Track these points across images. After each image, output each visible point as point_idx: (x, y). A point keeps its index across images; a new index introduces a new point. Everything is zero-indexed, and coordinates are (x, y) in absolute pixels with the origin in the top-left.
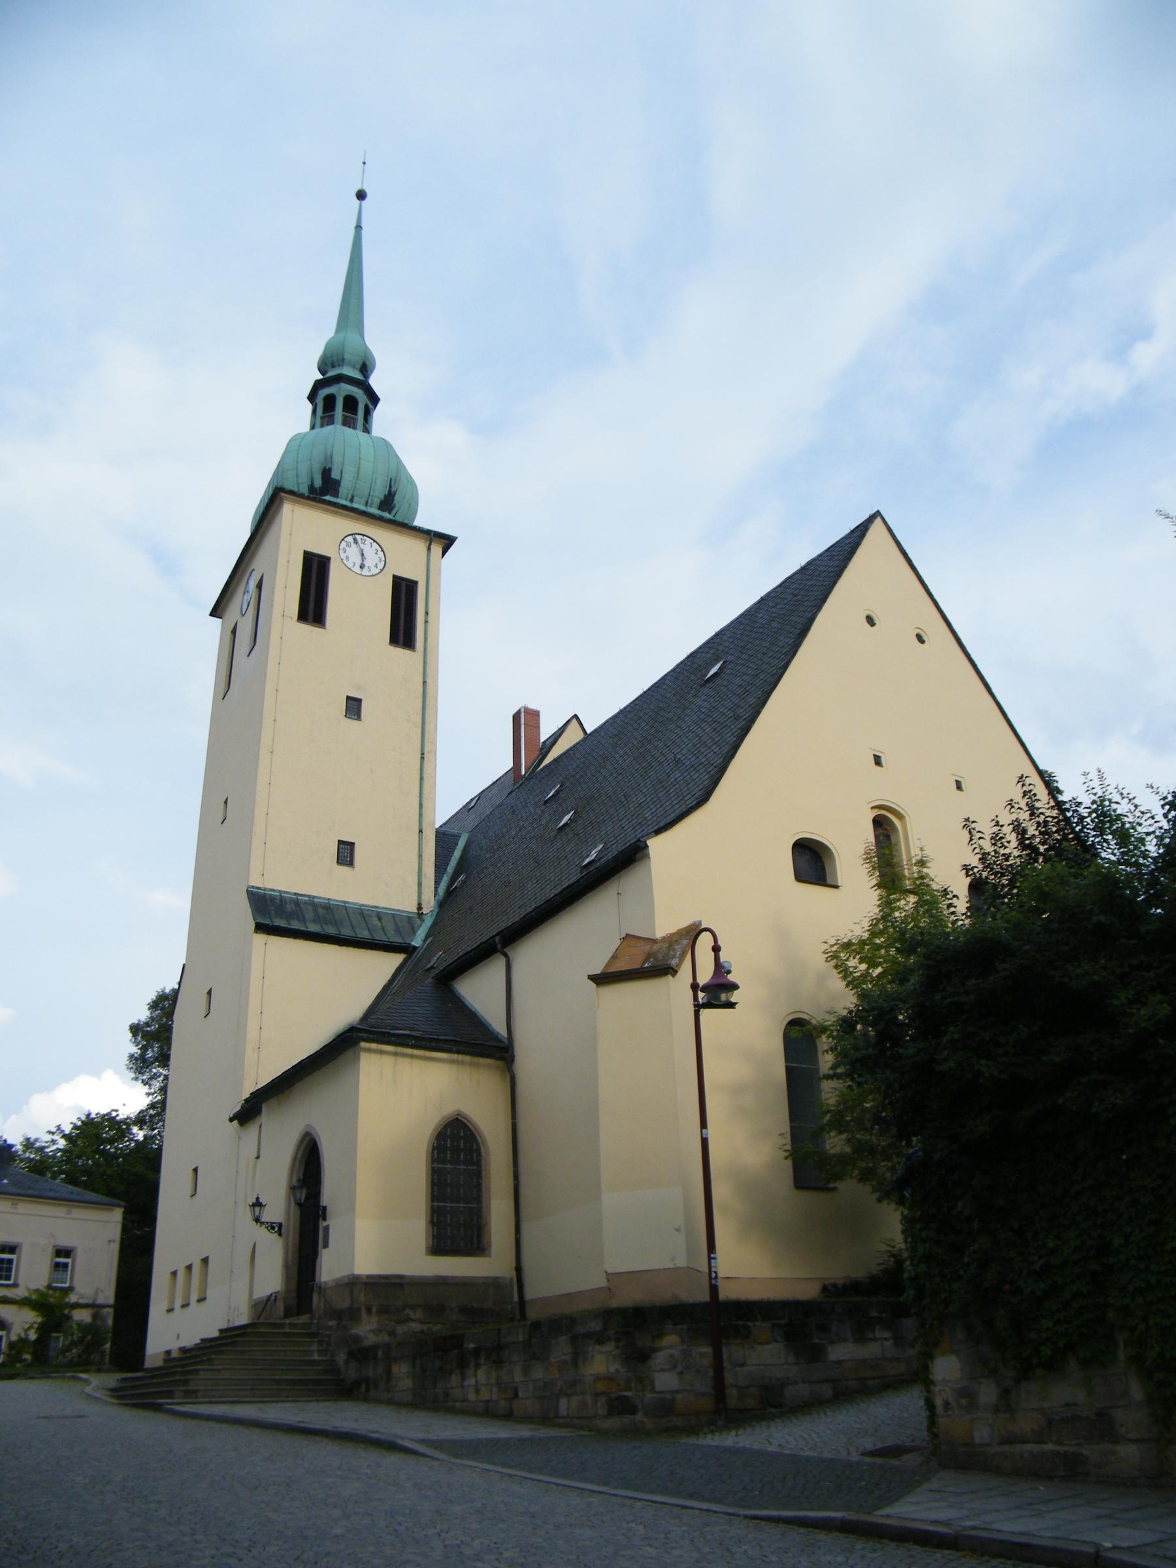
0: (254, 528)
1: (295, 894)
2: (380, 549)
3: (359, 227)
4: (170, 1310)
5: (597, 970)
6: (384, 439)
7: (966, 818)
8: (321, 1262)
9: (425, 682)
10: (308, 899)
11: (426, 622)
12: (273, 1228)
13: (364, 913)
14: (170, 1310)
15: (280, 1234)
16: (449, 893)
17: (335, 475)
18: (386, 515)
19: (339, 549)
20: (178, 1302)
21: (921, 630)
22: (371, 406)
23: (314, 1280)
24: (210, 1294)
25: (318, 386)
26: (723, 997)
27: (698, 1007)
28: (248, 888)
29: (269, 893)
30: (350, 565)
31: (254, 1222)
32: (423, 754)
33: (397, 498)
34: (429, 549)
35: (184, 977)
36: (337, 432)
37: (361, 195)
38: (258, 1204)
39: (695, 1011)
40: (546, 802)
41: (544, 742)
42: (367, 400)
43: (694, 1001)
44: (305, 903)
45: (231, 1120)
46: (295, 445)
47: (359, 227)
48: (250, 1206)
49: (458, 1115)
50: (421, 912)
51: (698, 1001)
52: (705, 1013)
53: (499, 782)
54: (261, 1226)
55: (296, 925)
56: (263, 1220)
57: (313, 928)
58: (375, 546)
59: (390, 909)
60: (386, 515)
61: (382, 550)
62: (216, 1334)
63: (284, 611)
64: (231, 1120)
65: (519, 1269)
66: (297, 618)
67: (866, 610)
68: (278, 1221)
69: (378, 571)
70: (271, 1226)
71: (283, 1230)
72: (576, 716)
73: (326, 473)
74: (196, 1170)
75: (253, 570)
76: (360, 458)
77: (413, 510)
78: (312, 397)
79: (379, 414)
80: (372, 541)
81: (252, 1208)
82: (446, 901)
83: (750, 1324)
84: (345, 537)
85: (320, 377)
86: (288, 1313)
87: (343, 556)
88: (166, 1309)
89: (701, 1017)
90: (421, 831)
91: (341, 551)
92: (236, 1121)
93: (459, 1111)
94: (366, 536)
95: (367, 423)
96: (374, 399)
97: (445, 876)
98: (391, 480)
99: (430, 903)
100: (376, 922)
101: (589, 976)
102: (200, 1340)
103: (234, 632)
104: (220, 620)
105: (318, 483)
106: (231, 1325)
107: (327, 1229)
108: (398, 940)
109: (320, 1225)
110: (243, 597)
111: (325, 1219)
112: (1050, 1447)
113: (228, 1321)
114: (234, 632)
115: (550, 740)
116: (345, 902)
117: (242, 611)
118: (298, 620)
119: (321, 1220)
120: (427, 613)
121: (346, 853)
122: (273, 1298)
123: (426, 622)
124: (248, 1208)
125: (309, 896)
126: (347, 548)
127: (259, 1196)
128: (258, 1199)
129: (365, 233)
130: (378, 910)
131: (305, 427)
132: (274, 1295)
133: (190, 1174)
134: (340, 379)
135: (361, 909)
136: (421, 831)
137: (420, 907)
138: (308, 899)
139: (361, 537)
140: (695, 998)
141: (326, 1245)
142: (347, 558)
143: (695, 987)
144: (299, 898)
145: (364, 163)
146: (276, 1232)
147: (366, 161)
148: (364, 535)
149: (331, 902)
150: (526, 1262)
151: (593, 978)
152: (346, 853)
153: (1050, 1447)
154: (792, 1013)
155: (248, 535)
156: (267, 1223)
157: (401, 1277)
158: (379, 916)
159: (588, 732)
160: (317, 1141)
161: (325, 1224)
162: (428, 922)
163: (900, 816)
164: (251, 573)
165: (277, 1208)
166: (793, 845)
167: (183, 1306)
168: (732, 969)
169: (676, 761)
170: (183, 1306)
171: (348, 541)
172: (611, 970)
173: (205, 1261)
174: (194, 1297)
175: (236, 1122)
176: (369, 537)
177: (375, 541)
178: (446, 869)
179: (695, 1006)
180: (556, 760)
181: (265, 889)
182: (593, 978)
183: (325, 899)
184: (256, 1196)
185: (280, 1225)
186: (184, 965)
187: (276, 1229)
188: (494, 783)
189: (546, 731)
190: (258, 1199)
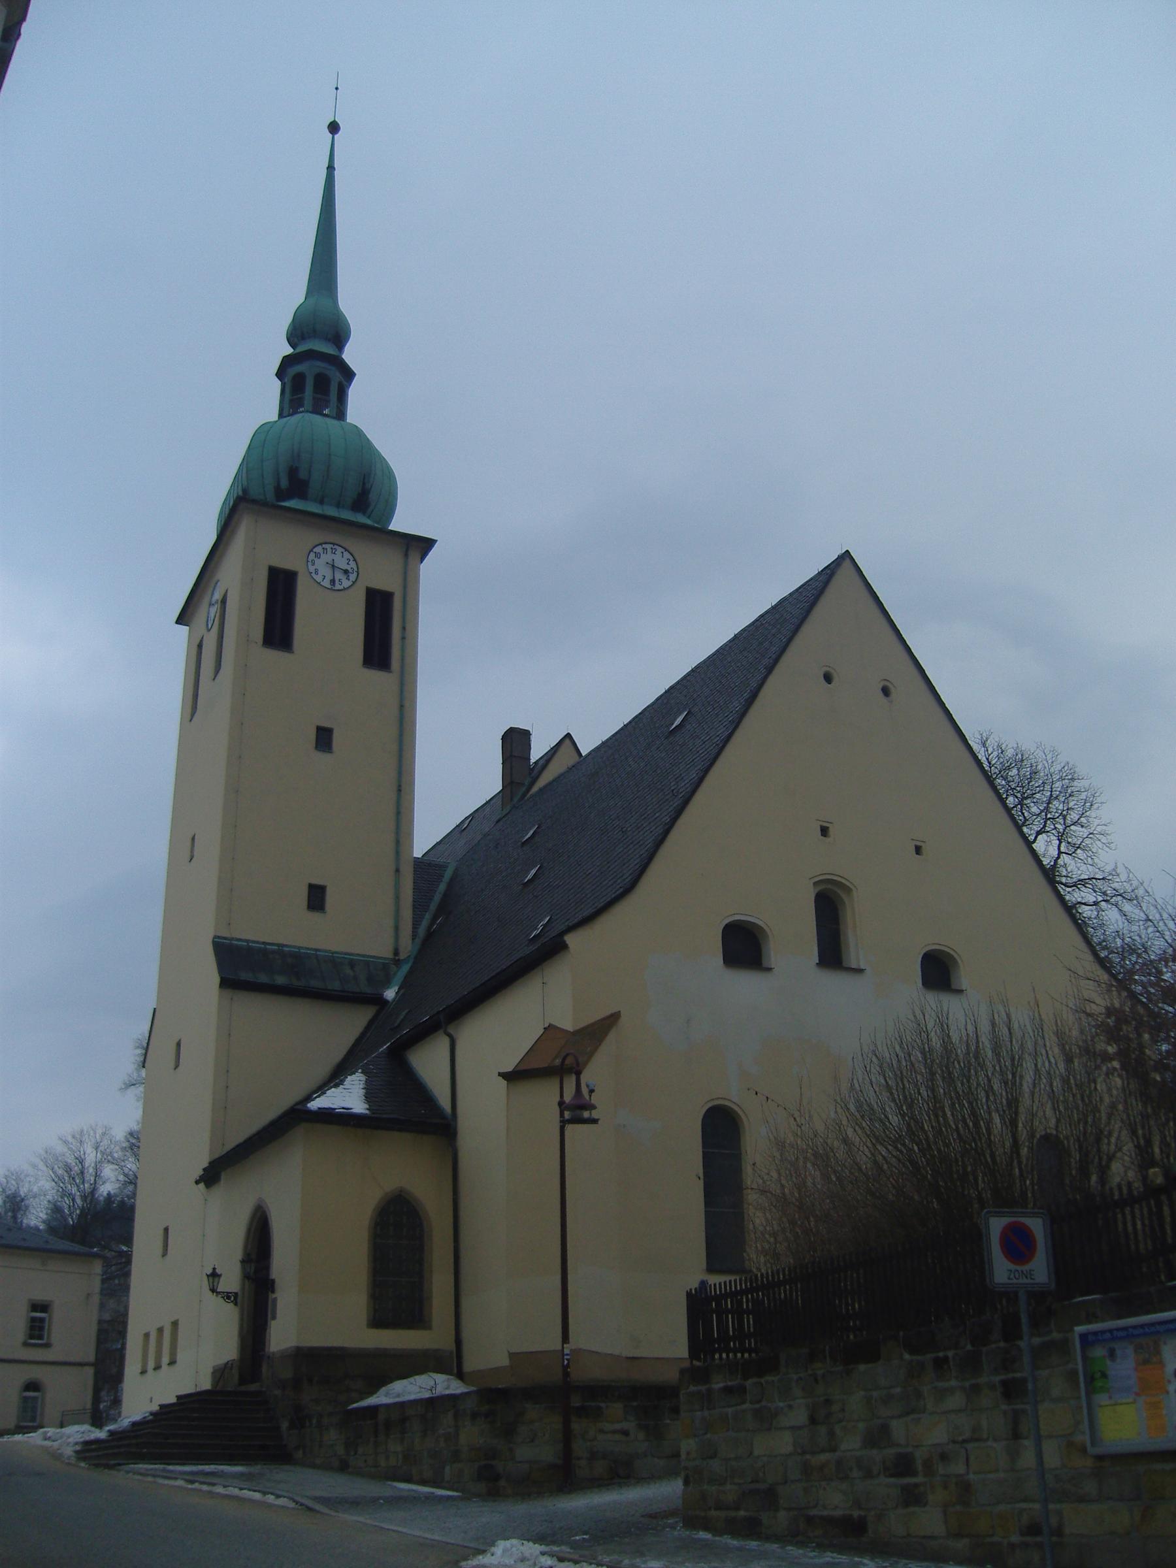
0: (219, 528)
1: (264, 943)
2: (352, 559)
3: (331, 168)
4: (143, 1372)
5: (509, 1068)
6: (357, 427)
7: (209, 1271)
8: (270, 1333)
9: (402, 706)
10: (276, 947)
11: (403, 638)
12: (229, 1298)
13: (335, 962)
14: (143, 1372)
15: (236, 1304)
16: (430, 935)
17: (303, 475)
18: (361, 519)
19: (308, 561)
20: (151, 1364)
21: (890, 682)
22: (345, 383)
23: (263, 1350)
24: (179, 1357)
25: (287, 362)
26: (586, 1114)
27: (564, 1123)
28: (214, 938)
29: (236, 942)
30: (319, 578)
31: (211, 1293)
32: (400, 786)
33: (373, 496)
34: (406, 555)
35: (154, 1026)
36: (308, 422)
37: (334, 128)
38: (214, 1275)
39: (561, 1126)
40: (524, 844)
41: (535, 763)
42: (341, 377)
43: (561, 1117)
44: (273, 952)
45: (197, 1182)
46: (262, 439)
47: (331, 168)
48: (208, 1276)
49: (401, 1191)
50: (397, 958)
51: (564, 1117)
52: (569, 1128)
53: (492, 802)
54: (217, 1296)
55: (263, 978)
56: (218, 1290)
57: (280, 980)
58: (347, 555)
59: (364, 956)
60: (361, 519)
61: (355, 560)
62: (174, 1400)
63: (248, 636)
64: (197, 1182)
65: (458, 1342)
66: (262, 643)
67: (824, 666)
68: (234, 1291)
69: (350, 583)
70: (227, 1296)
71: (239, 1300)
72: (568, 736)
73: (293, 472)
74: (166, 1230)
75: (218, 581)
76: (330, 455)
77: (389, 509)
78: (280, 374)
79: (355, 393)
80: (343, 550)
81: (211, 1279)
82: (428, 942)
83: (603, 1405)
84: (314, 547)
85: (289, 350)
86: (243, 1381)
87: (312, 569)
88: (140, 1371)
89: (567, 1133)
90: (397, 870)
91: (310, 564)
92: (203, 1184)
93: (401, 1187)
94: (337, 545)
95: (341, 404)
96: (349, 375)
97: (427, 913)
98: (364, 475)
99: (408, 947)
100: (348, 971)
101: (499, 1073)
102: (512, 1356)
103: (200, 646)
104: (188, 628)
105: (284, 483)
106: (198, 1390)
107: (275, 1300)
108: (368, 990)
109: (270, 1296)
110: (206, 612)
111: (273, 1292)
112: (742, 1513)
113: (196, 1385)
114: (200, 646)
115: (545, 758)
116: (317, 950)
117: (207, 625)
118: (263, 645)
119: (270, 1293)
120: (404, 628)
121: (316, 898)
122: (230, 1365)
123: (403, 638)
124: (205, 1278)
125: (278, 945)
126: (316, 560)
127: (216, 1267)
128: (214, 1269)
129: (337, 174)
130: (351, 957)
131: (273, 415)
132: (230, 1363)
133: (161, 1232)
134: (311, 355)
135: (333, 957)
136: (397, 870)
137: (396, 952)
138: (276, 947)
139: (332, 546)
140: (562, 1115)
141: (274, 1318)
142: (316, 572)
143: (561, 1104)
144: (268, 947)
145: (337, 89)
146: (232, 1302)
147: (339, 87)
148: (334, 544)
149: (302, 951)
150: (466, 1335)
151: (505, 1076)
152: (316, 898)
153: (742, 1513)
154: (708, 1101)
155: (213, 537)
156: (224, 1292)
157: (342, 1349)
158: (352, 964)
159: (584, 752)
160: (269, 1216)
161: (274, 1296)
162: (405, 968)
163: (848, 890)
164: (216, 583)
165: (232, 1280)
166: (724, 928)
167: (155, 1369)
168: (595, 1089)
169: (623, 832)
170: (155, 1369)
171: (317, 551)
172: (518, 1069)
173: (175, 1324)
174: (165, 1360)
175: (202, 1185)
176: (340, 546)
177: (346, 550)
178: (429, 906)
179: (561, 1122)
180: (541, 790)
181: (232, 939)
182: (505, 1076)
183: (294, 947)
184: (213, 1267)
185: (236, 1294)
186: (155, 1009)
187: (232, 1299)
188: (487, 803)
189: (537, 752)
190: (214, 1269)
